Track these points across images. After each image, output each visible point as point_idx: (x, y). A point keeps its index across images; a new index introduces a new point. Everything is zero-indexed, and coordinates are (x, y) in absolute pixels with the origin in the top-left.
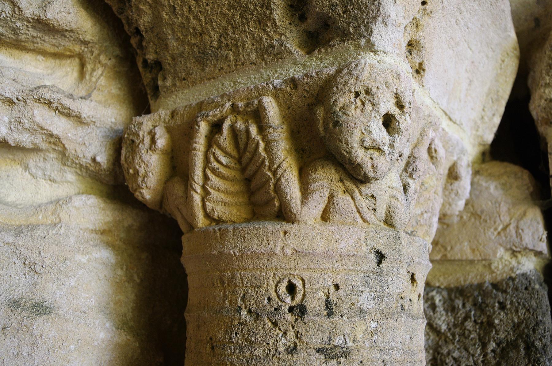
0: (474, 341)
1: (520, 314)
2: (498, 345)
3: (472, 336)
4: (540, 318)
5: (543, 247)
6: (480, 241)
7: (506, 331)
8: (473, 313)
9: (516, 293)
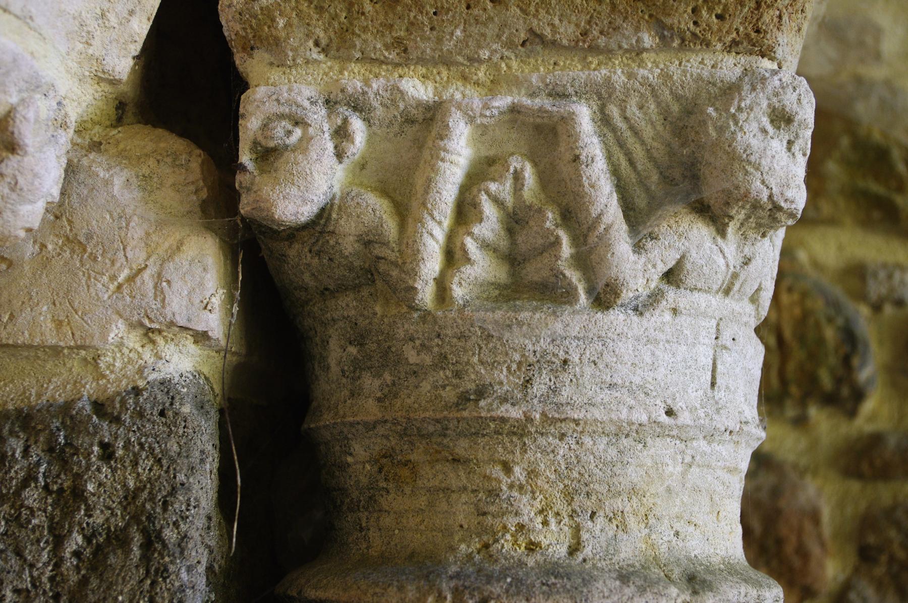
0: (37, 534)
1: (140, 470)
2: (88, 539)
3: (35, 521)
4: (181, 477)
5: (215, 322)
6: (76, 304)
7: (109, 508)
8: (42, 469)
9: (139, 422)
